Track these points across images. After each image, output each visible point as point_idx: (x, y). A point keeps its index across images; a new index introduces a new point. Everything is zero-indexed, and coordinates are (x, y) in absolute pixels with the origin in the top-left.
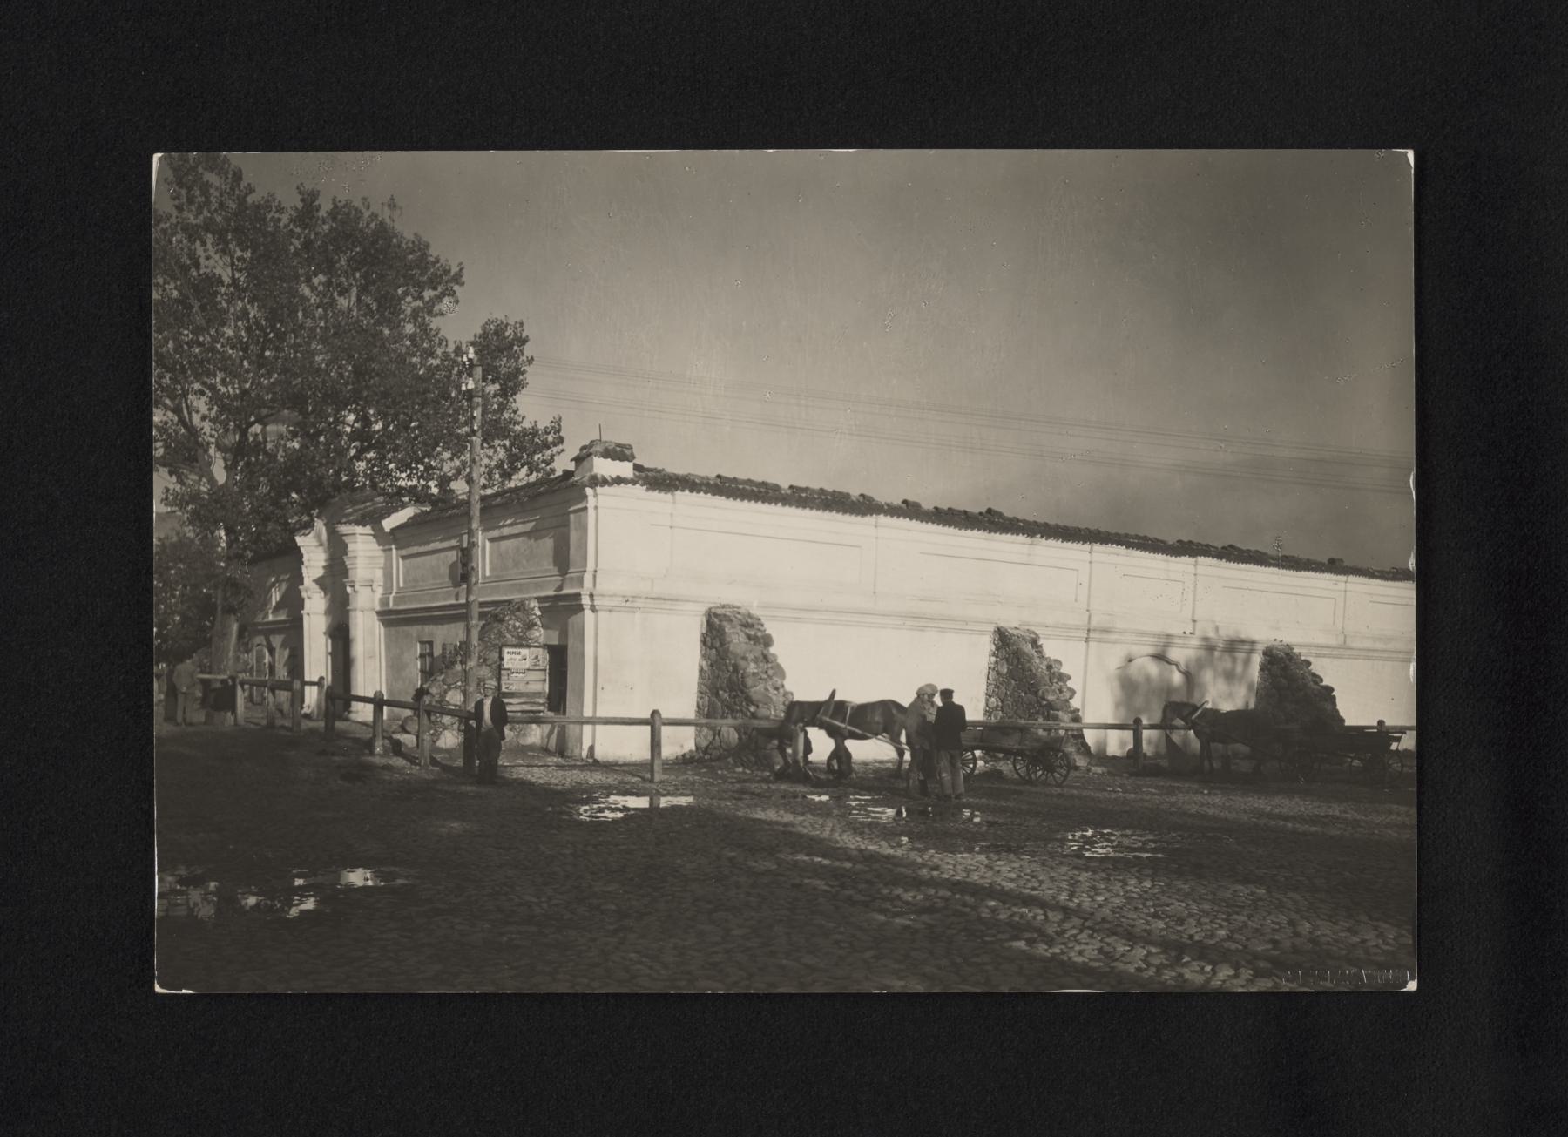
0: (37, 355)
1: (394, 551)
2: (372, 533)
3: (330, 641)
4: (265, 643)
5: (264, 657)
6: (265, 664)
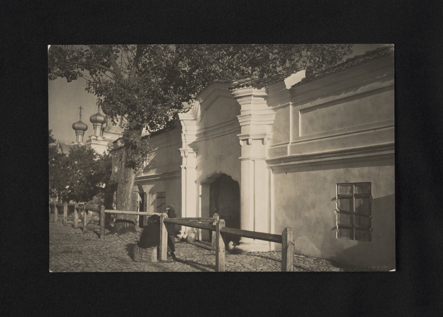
0: (5, 105)
1: (291, 107)
2: (266, 94)
3: (200, 187)
4: (138, 190)
5: (136, 197)
6: (137, 202)
